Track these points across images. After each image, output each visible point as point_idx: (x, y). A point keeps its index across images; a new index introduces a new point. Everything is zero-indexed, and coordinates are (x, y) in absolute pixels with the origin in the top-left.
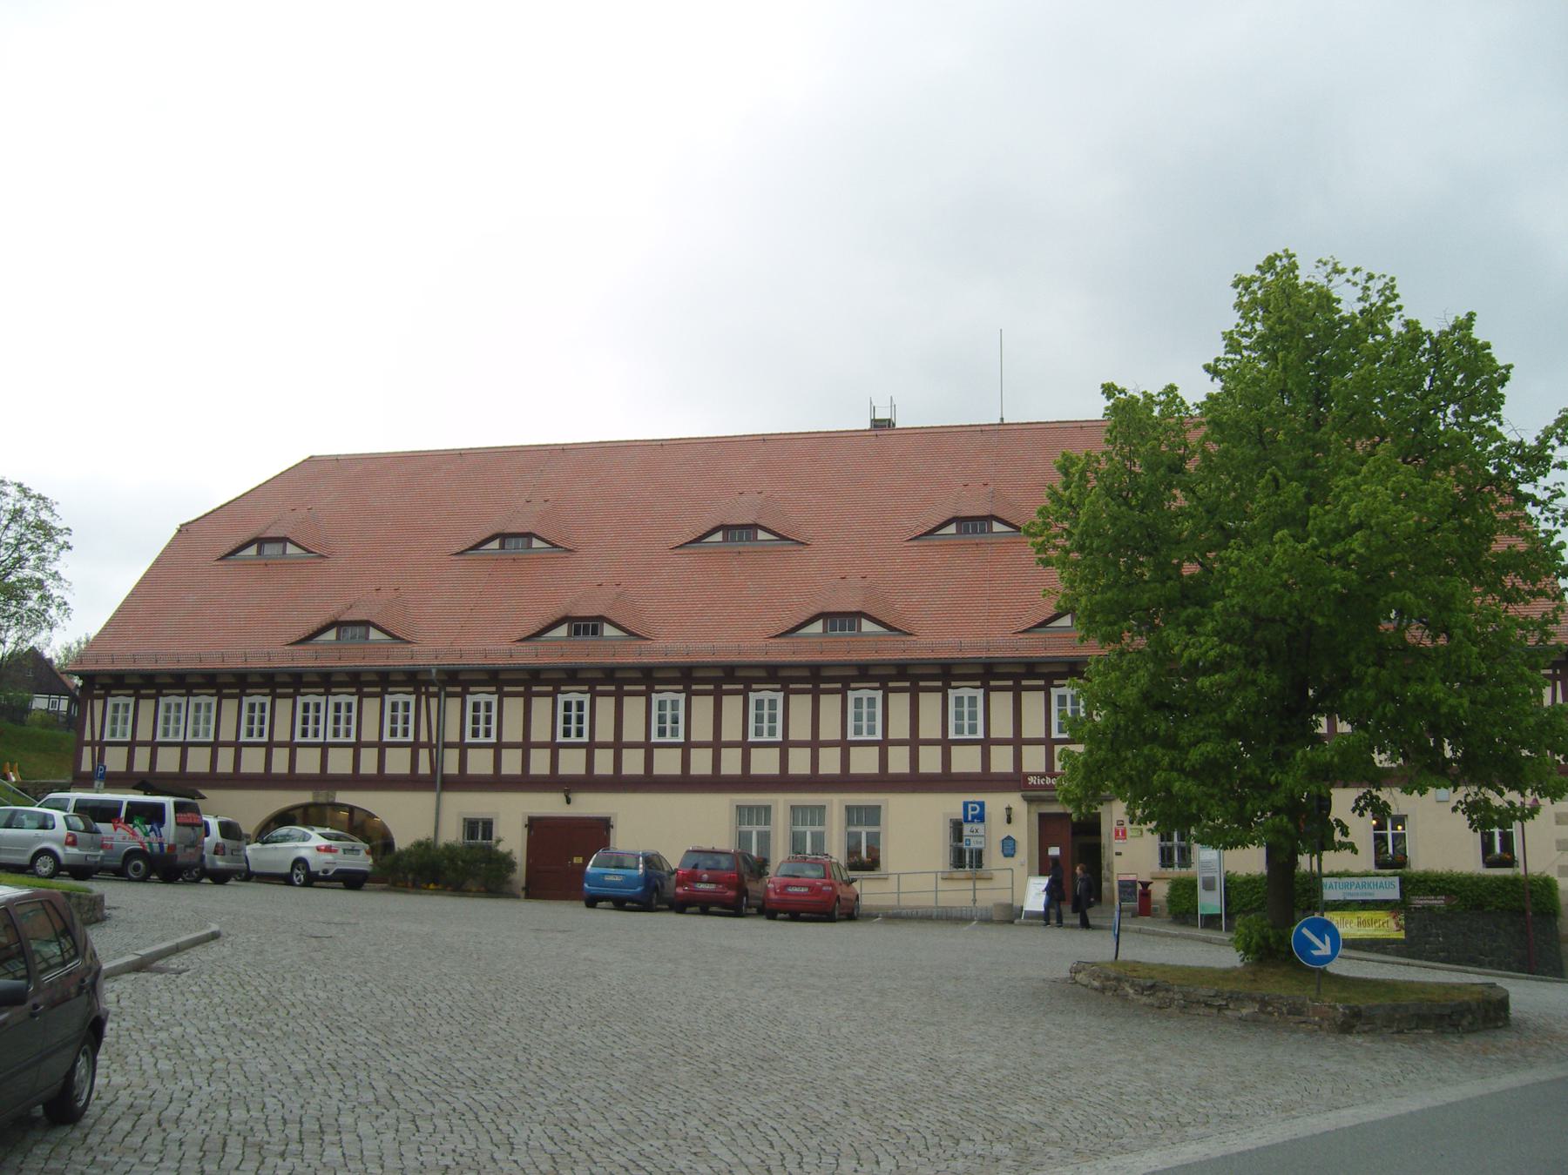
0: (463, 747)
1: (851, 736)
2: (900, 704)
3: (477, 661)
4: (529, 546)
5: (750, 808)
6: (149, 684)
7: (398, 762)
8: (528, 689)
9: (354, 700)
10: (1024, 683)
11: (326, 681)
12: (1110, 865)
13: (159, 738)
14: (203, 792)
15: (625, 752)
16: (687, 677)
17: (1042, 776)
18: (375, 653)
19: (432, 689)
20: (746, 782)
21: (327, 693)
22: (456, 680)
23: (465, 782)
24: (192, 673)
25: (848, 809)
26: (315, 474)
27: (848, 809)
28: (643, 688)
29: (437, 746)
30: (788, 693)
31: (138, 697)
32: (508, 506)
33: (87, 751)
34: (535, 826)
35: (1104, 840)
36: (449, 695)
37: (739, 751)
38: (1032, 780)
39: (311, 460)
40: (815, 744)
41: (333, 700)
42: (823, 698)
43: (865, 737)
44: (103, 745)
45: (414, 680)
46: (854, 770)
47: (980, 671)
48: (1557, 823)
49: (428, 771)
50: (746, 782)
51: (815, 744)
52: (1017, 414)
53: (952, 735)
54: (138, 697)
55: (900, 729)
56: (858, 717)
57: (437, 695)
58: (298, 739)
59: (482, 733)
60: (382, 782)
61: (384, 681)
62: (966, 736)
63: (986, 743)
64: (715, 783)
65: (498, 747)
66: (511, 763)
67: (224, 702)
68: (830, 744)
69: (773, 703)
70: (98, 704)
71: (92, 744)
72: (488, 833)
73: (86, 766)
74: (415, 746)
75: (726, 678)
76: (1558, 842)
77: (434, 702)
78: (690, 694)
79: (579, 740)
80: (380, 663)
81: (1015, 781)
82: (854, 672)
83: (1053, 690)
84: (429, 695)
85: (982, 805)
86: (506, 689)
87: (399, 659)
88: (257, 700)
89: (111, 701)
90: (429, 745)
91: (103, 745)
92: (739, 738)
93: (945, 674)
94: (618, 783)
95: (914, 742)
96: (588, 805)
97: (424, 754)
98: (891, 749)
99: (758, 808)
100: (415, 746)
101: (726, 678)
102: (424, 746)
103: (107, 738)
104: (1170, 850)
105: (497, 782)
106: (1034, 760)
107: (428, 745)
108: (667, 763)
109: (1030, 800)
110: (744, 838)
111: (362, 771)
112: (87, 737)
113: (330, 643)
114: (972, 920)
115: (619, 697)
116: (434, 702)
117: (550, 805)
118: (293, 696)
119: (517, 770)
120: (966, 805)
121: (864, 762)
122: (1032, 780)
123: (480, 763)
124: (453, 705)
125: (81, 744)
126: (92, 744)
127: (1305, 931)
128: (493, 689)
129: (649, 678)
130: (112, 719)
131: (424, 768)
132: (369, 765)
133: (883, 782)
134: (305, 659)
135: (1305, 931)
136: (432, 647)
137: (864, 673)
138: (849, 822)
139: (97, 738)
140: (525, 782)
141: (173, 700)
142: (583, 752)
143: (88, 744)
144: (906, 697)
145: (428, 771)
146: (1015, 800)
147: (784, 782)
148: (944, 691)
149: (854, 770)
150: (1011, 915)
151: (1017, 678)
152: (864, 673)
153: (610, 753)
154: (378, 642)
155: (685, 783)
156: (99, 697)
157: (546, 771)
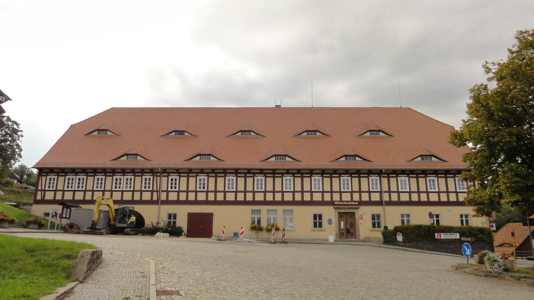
0: (167, 192)
1: (284, 190)
2: (270, 180)
3: (173, 166)
4: (106, 134)
5: (255, 210)
6: (62, 172)
7: (147, 196)
9: (133, 177)
10: (333, 175)
11: (124, 172)
12: (358, 227)
14: (80, 205)
15: (218, 193)
16: (236, 172)
17: (339, 202)
18: (139, 163)
19: (158, 174)
20: (254, 202)
21: (124, 175)
22: (166, 172)
23: (167, 202)
24: (79, 169)
25: (252, 210)
26: (114, 112)
27: (252, 210)
29: (159, 191)
30: (266, 177)
31: (58, 176)
32: (175, 123)
33: (39, 193)
34: (192, 217)
35: (356, 220)
36: (163, 176)
37: (110, 193)
38: (336, 203)
41: (78, 177)
42: (420, 179)
43: (259, 190)
44: (45, 191)
45: (152, 172)
46: (170, 199)
47: (444, 172)
50: (254, 202)
51: (274, 192)
52: (317, 104)
53: (227, 190)
54: (58, 176)
55: (356, 188)
56: (286, 184)
57: (160, 176)
58: (114, 189)
59: (173, 188)
60: (141, 202)
61: (143, 172)
63: (410, 193)
64: (245, 203)
66: (183, 197)
67: (89, 177)
69: (261, 180)
70: (44, 178)
71: (41, 190)
72: (175, 217)
73: (39, 197)
74: (152, 191)
75: (249, 172)
77: (158, 178)
78: (237, 177)
80: (141, 166)
81: (331, 203)
82: (285, 172)
84: (157, 176)
86: (181, 175)
87: (148, 165)
88: (100, 177)
89: (48, 177)
90: (157, 191)
91: (45, 191)
92: (166, 189)
93: (311, 172)
94: (215, 202)
97: (155, 194)
98: (296, 193)
99: (257, 210)
100: (152, 191)
101: (249, 172)
102: (155, 191)
103: (47, 189)
104: (375, 223)
105: (178, 202)
106: (336, 197)
107: (157, 191)
108: (230, 197)
109: (336, 208)
110: (403, 221)
111: (180, 199)
112: (40, 188)
113: (418, 162)
115: (216, 177)
116: (158, 178)
118: (112, 176)
119: (251, 199)
121: (288, 197)
123: (173, 197)
124: (164, 179)
125: (37, 190)
126: (41, 190)
127: (465, 247)
129: (225, 172)
130: (45, 182)
131: (155, 198)
132: (137, 197)
133: (294, 203)
134: (116, 165)
135: (465, 247)
136: (157, 163)
137: (288, 172)
138: (284, 214)
139: (43, 189)
140: (187, 202)
141: (71, 177)
143: (40, 190)
144: (386, 179)
147: (265, 203)
148: (310, 177)
149: (314, 199)
150: (324, 242)
151: (417, 174)
152: (288, 172)
154: (214, 161)
155: (236, 202)
156: (44, 176)
157: (280, 199)
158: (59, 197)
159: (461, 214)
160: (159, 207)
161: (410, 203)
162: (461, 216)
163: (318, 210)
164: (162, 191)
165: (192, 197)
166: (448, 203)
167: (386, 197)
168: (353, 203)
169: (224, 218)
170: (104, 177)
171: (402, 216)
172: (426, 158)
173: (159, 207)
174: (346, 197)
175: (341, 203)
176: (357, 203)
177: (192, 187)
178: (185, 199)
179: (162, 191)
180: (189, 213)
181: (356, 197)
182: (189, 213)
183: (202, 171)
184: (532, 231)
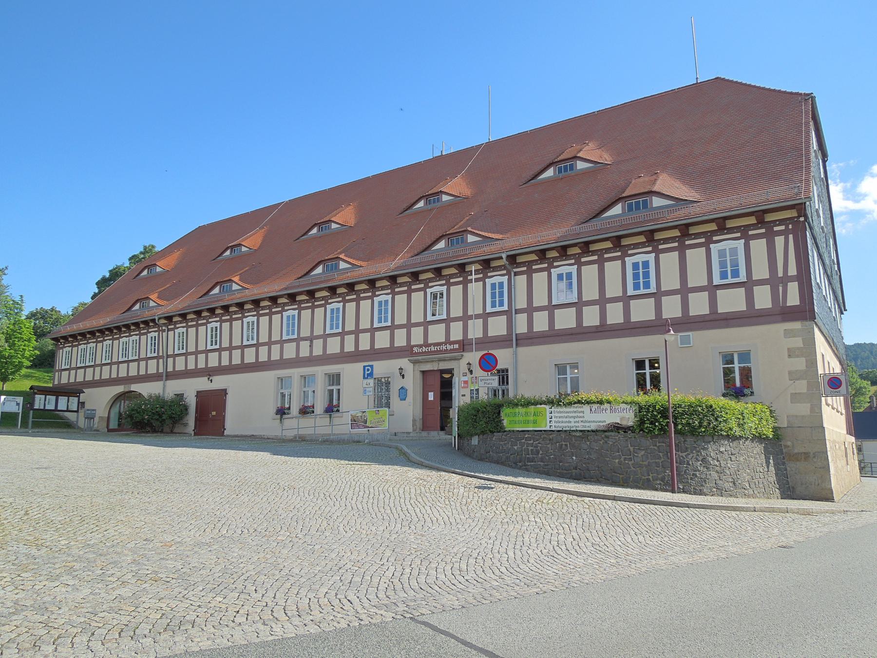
8: (271, 310)
9: (651, 257)
13: (717, 281)
17: (420, 346)
20: (283, 364)
28: (619, 254)
34: (199, 394)
36: (516, 274)
38: (415, 349)
39: (201, 231)
40: (409, 326)
48: (790, 356)
49: (797, 302)
50: (283, 364)
53: (717, 281)
62: (730, 280)
64: (268, 366)
65: (657, 296)
68: (540, 309)
76: (790, 373)
79: (501, 309)
81: (407, 351)
83: (552, 270)
85: (372, 366)
94: (231, 369)
95: (684, 291)
96: (219, 382)
106: (417, 336)
109: (414, 362)
114: (369, 444)
117: (202, 384)
119: (337, 350)
120: (364, 367)
122: (415, 349)
128: (650, 249)
142: (742, 291)
145: (797, 302)
146: (404, 363)
153: (460, 324)
157: (621, 320)
158: (400, 340)
159: (640, 357)
160: (515, 354)
161: (579, 333)
162: (640, 364)
163: (646, 346)
164: (517, 311)
165: (699, 305)
166: (687, 323)
167: (591, 317)
168: (449, 347)
169: (249, 399)
170: (651, 257)
171: (640, 364)
172: (458, 240)
173: (515, 354)
174: (437, 334)
175: (424, 349)
176: (456, 346)
177: (613, 289)
178: (706, 311)
179: (517, 311)
180: (198, 392)
181: (457, 333)
182: (198, 392)
183: (722, 225)
184: (863, 406)
